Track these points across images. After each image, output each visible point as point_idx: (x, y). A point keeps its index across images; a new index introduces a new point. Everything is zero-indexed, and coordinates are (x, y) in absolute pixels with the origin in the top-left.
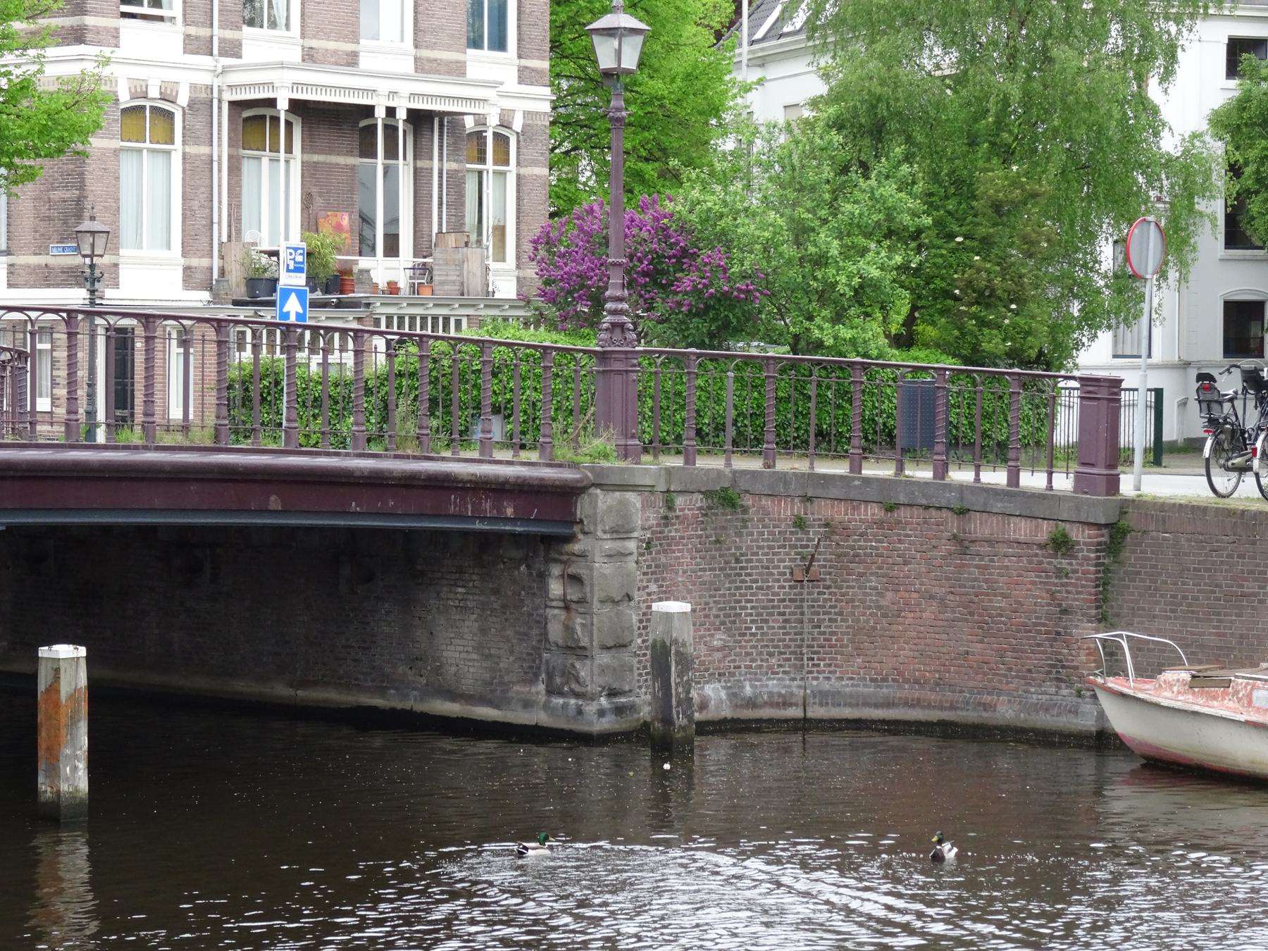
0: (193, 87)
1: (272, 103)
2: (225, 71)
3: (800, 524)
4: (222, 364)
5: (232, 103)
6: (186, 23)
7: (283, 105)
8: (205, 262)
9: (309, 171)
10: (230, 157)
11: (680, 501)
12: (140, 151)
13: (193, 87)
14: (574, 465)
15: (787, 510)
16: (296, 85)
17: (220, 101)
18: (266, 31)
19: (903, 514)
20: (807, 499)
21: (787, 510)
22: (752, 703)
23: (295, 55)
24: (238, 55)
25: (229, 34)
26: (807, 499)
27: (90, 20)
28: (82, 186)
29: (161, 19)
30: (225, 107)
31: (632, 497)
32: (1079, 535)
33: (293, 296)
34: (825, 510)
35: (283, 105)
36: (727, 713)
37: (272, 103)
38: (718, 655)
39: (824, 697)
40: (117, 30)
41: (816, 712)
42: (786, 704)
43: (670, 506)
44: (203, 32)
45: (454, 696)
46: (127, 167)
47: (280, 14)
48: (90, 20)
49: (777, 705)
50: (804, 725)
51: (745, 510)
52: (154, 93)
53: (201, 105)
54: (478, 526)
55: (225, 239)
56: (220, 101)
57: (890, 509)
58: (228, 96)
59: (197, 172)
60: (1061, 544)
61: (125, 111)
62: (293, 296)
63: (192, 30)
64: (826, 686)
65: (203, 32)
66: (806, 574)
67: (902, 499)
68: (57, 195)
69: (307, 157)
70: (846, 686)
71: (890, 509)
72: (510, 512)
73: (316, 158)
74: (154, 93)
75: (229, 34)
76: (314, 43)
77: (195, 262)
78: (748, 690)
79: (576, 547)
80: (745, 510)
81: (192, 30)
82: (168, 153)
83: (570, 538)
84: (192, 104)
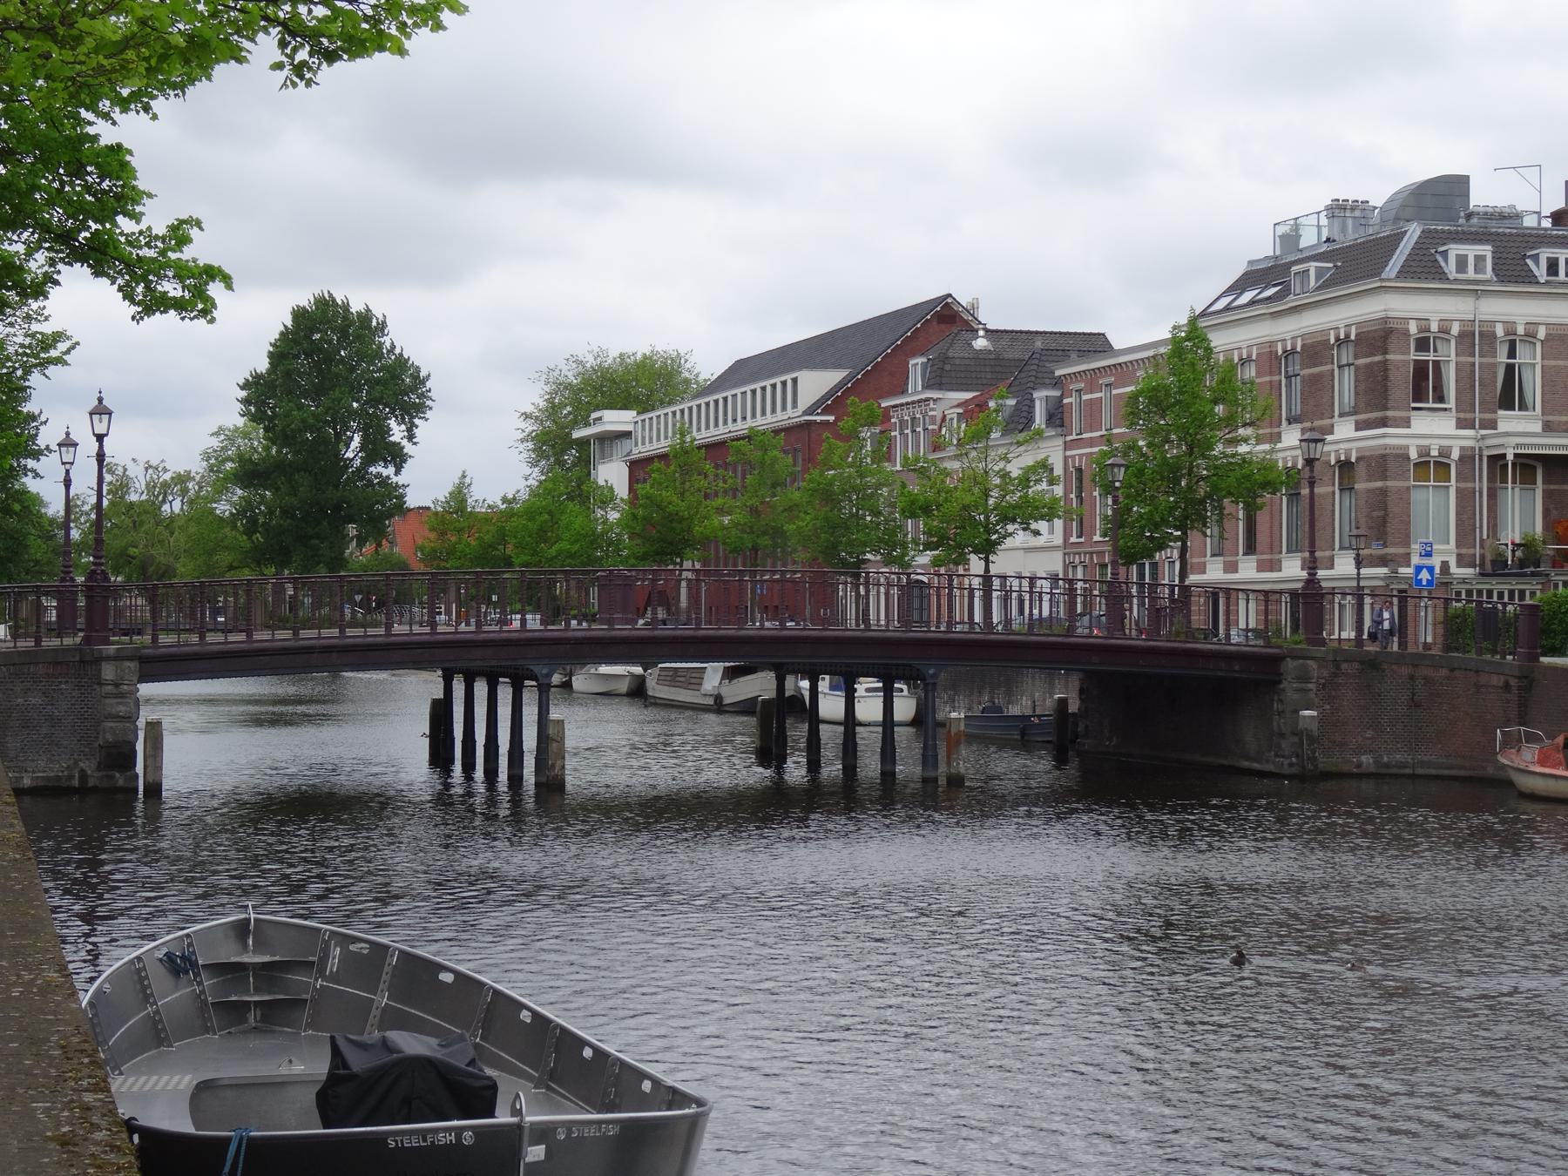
0: (1462, 448)
1: (1504, 456)
2: (1483, 437)
3: (1412, 678)
4: (1446, 609)
5: (1489, 457)
6: (1457, 411)
7: (1510, 457)
8: (1471, 551)
9: (1548, 495)
10: (1488, 489)
11: (1344, 666)
12: (1428, 487)
13: (1462, 448)
14: (1280, 647)
15: (1405, 671)
16: (1517, 446)
17: (1481, 456)
18: (1517, 412)
19: (1457, 673)
20: (1416, 666)
21: (1405, 671)
22: (1387, 766)
23: (1537, 427)
24: (1495, 428)
25: (1488, 416)
26: (1416, 666)
27: (1390, 413)
28: (1385, 509)
29: (1446, 409)
30: (1485, 460)
31: (1310, 662)
32: (1513, 682)
33: (1425, 570)
34: (1425, 671)
35: (1510, 457)
36: (1373, 770)
37: (1504, 456)
38: (1368, 742)
39: (1423, 764)
40: (1409, 418)
41: (1420, 771)
42: (1405, 767)
43: (1338, 667)
44: (1468, 416)
45: (1248, 758)
46: (1416, 496)
47: (1530, 405)
48: (1390, 413)
49: (1400, 767)
50: (1414, 777)
51: (1384, 671)
52: (1434, 453)
53: (1467, 458)
54: (1219, 674)
55: (1485, 537)
56: (1481, 456)
57: (1452, 670)
58: (1486, 453)
59: (1465, 499)
60: (1507, 686)
61: (1415, 464)
62: (1425, 570)
63: (1462, 415)
64: (1425, 759)
65: (1468, 416)
66: (1415, 704)
67: (1456, 665)
68: (1375, 514)
69: (1546, 487)
70: (1433, 758)
71: (1452, 670)
72: (1237, 668)
73: (1552, 487)
74: (1434, 453)
75: (1488, 416)
76: (1551, 418)
77: (1464, 551)
78: (1386, 759)
79: (1282, 686)
80: (1384, 671)
81: (1462, 415)
82: (1448, 487)
83: (1280, 682)
84: (1461, 458)
